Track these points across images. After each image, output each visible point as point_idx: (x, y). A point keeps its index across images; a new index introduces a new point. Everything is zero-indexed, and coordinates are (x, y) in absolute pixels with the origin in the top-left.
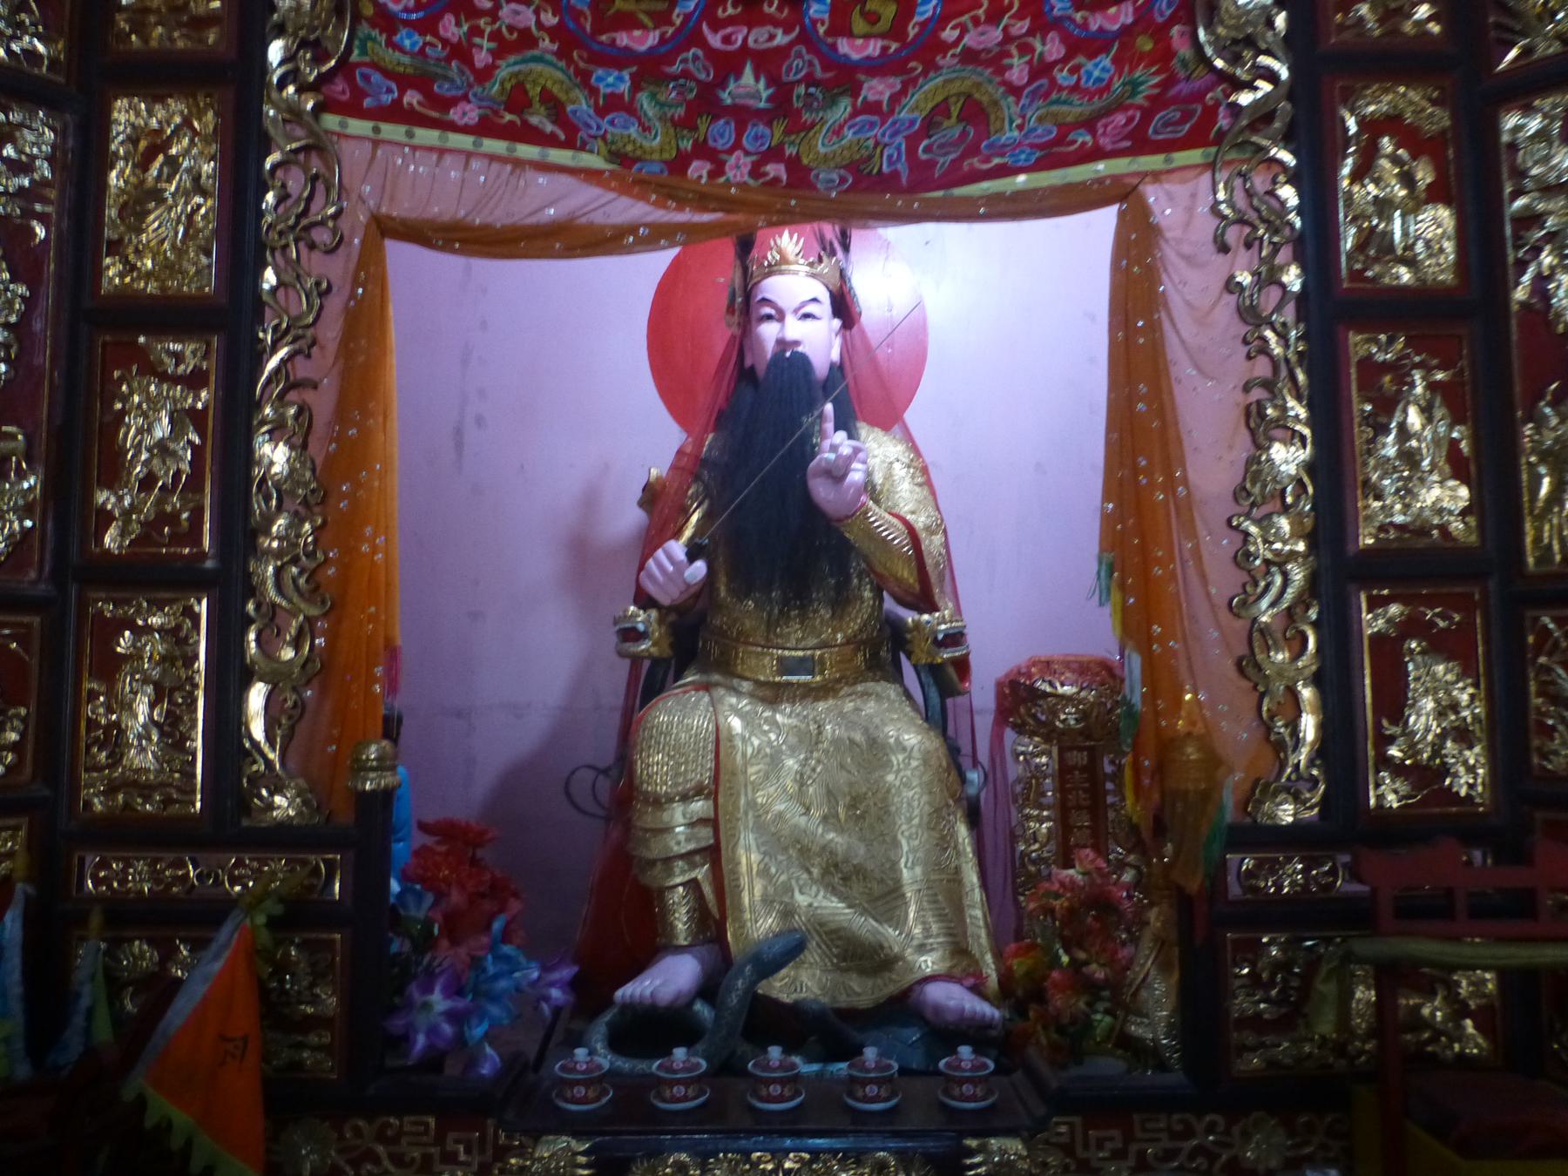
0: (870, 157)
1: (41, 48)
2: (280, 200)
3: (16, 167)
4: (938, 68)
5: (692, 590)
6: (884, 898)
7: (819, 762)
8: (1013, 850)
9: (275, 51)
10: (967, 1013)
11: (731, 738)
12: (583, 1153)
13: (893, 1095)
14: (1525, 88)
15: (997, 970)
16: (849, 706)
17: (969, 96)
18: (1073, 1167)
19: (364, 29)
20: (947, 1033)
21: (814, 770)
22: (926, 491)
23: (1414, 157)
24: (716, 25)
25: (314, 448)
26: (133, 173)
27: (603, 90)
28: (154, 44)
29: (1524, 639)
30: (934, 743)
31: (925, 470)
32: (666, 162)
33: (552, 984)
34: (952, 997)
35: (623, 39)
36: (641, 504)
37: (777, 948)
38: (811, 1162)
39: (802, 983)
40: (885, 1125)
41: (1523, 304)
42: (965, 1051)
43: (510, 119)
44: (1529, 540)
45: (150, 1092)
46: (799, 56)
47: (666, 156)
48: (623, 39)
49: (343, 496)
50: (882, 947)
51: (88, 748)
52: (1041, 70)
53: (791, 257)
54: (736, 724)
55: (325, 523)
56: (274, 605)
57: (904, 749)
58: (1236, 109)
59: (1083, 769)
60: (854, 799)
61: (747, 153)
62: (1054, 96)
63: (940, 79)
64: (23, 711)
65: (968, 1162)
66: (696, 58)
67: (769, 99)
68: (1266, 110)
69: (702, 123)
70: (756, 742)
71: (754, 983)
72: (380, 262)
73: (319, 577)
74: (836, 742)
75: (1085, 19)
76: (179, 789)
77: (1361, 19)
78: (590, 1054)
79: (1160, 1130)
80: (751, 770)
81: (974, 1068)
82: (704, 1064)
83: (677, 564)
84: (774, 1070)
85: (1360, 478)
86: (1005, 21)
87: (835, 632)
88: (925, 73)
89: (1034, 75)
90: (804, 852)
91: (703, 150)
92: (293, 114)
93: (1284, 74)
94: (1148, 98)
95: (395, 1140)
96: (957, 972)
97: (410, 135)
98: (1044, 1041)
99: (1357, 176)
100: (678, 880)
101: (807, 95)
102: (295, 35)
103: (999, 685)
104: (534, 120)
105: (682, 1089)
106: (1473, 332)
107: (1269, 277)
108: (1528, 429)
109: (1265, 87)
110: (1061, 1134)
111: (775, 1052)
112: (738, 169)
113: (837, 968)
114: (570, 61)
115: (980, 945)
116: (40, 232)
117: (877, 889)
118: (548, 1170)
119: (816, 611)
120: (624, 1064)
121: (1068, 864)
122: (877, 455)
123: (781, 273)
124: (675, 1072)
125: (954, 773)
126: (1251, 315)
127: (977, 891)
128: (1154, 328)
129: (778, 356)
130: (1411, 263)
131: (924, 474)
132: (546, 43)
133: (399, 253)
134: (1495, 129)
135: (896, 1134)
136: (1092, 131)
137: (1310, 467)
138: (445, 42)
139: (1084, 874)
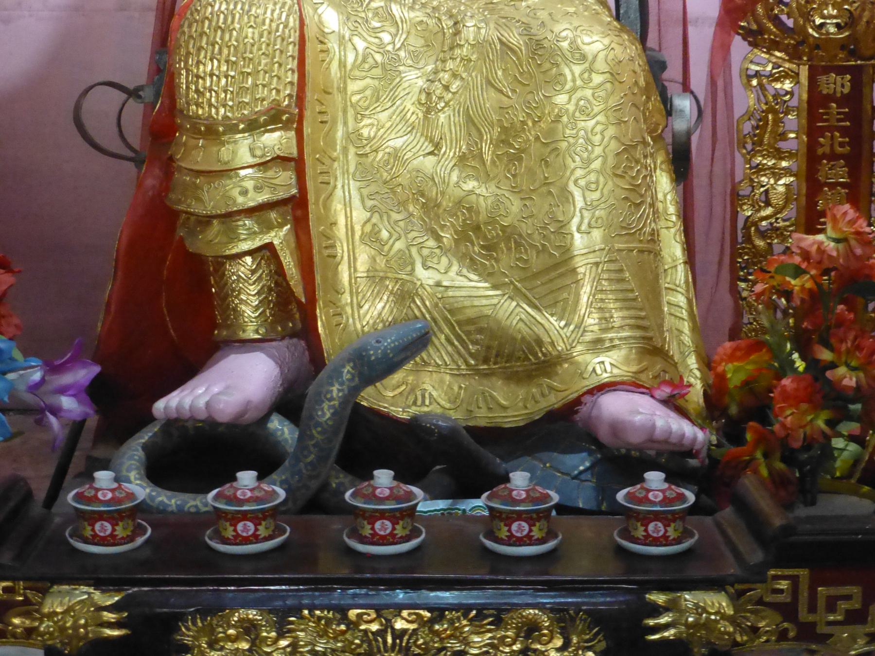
6: (547, 275)
7: (455, 75)
8: (735, 215)
10: (658, 434)
12: (110, 609)
13: (550, 534)
15: (703, 379)
18: (792, 634)
20: (624, 461)
21: (446, 88)
30: (627, 50)
33: (63, 390)
34: (638, 413)
37: (389, 342)
38: (432, 621)
39: (429, 393)
40: (540, 574)
42: (655, 479)
50: (539, 342)
57: (584, 57)
59: (843, 101)
60: (504, 130)
65: (651, 622)
70: (360, 45)
71: (355, 391)
74: (479, 45)
78: (117, 479)
80: (353, 86)
81: (666, 501)
82: (282, 494)
84: (382, 500)
90: (431, 208)
96: (646, 379)
98: (764, 472)
100: (245, 246)
105: (251, 526)
110: (781, 591)
111: (384, 478)
115: (681, 343)
117: (536, 262)
118: (63, 629)
120: (170, 500)
121: (811, 229)
124: (241, 502)
125: (655, 98)
127: (681, 268)
135: (552, 586)
139: (837, 241)
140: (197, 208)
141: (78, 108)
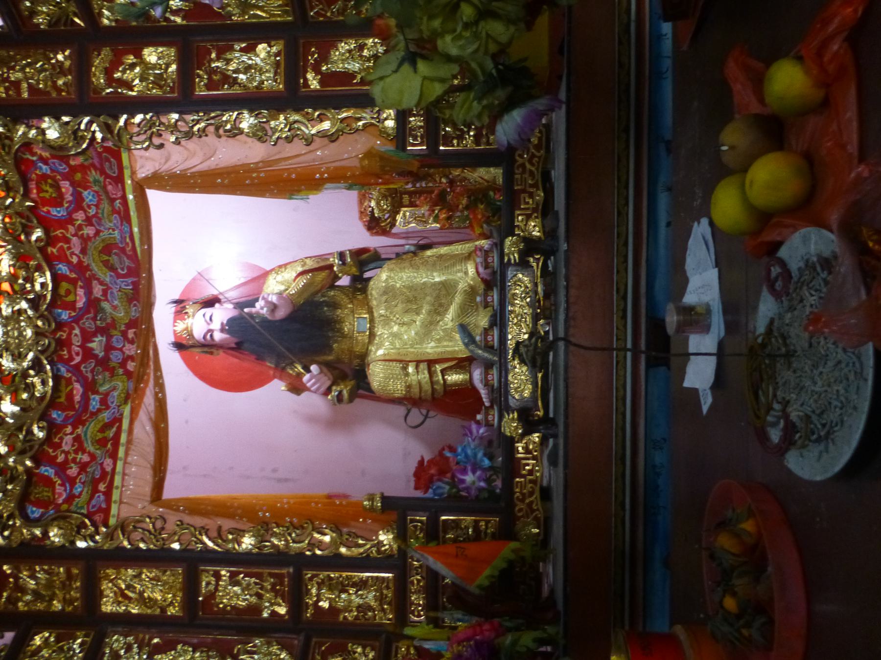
0: (126, 294)
1: (79, 641)
3: (129, 648)
4: (88, 265)
5: (325, 370)
6: (447, 288)
9: (81, 544)
11: (385, 355)
14: (92, 18)
16: (374, 303)
17: (101, 252)
19: (73, 508)
23: (122, 63)
24: (71, 359)
26: (133, 603)
27: (98, 406)
28: (78, 595)
29: (321, 22)
31: (280, 267)
32: (128, 379)
33: (478, 432)
35: (77, 398)
36: (299, 394)
41: (183, 20)
43: (110, 444)
44: (279, 19)
45: (477, 582)
46: (84, 323)
47: (126, 380)
48: (77, 398)
49: (264, 515)
51: (366, 619)
52: (89, 221)
53: (184, 326)
54: (380, 352)
55: (275, 523)
56: (309, 543)
58: (103, 139)
59: (410, 196)
61: (124, 346)
62: (100, 215)
63: (93, 264)
66: (85, 367)
67: (102, 336)
68: (104, 127)
69: (112, 364)
72: (170, 501)
73: (297, 525)
74: (386, 310)
75: (67, 202)
76: (383, 583)
77: (64, 84)
80: (398, 346)
83: (313, 377)
85: (255, 90)
86: (69, 236)
88: (91, 270)
89: (92, 225)
90: (431, 323)
91: (123, 364)
92: (110, 536)
93: (86, 119)
94: (101, 176)
95: (523, 495)
97: (117, 488)
100: (440, 377)
101: (100, 320)
102: (75, 536)
103: (372, 234)
104: (111, 435)
106: (199, 37)
109: (94, 127)
112: (131, 350)
114: (86, 420)
116: (156, 641)
117: (444, 292)
119: (338, 316)
122: (273, 287)
123: (192, 331)
126: (189, 135)
128: (193, 175)
129: (228, 332)
130: (168, 65)
132: (79, 431)
136: (115, 199)
137: (251, 111)
138: (79, 474)
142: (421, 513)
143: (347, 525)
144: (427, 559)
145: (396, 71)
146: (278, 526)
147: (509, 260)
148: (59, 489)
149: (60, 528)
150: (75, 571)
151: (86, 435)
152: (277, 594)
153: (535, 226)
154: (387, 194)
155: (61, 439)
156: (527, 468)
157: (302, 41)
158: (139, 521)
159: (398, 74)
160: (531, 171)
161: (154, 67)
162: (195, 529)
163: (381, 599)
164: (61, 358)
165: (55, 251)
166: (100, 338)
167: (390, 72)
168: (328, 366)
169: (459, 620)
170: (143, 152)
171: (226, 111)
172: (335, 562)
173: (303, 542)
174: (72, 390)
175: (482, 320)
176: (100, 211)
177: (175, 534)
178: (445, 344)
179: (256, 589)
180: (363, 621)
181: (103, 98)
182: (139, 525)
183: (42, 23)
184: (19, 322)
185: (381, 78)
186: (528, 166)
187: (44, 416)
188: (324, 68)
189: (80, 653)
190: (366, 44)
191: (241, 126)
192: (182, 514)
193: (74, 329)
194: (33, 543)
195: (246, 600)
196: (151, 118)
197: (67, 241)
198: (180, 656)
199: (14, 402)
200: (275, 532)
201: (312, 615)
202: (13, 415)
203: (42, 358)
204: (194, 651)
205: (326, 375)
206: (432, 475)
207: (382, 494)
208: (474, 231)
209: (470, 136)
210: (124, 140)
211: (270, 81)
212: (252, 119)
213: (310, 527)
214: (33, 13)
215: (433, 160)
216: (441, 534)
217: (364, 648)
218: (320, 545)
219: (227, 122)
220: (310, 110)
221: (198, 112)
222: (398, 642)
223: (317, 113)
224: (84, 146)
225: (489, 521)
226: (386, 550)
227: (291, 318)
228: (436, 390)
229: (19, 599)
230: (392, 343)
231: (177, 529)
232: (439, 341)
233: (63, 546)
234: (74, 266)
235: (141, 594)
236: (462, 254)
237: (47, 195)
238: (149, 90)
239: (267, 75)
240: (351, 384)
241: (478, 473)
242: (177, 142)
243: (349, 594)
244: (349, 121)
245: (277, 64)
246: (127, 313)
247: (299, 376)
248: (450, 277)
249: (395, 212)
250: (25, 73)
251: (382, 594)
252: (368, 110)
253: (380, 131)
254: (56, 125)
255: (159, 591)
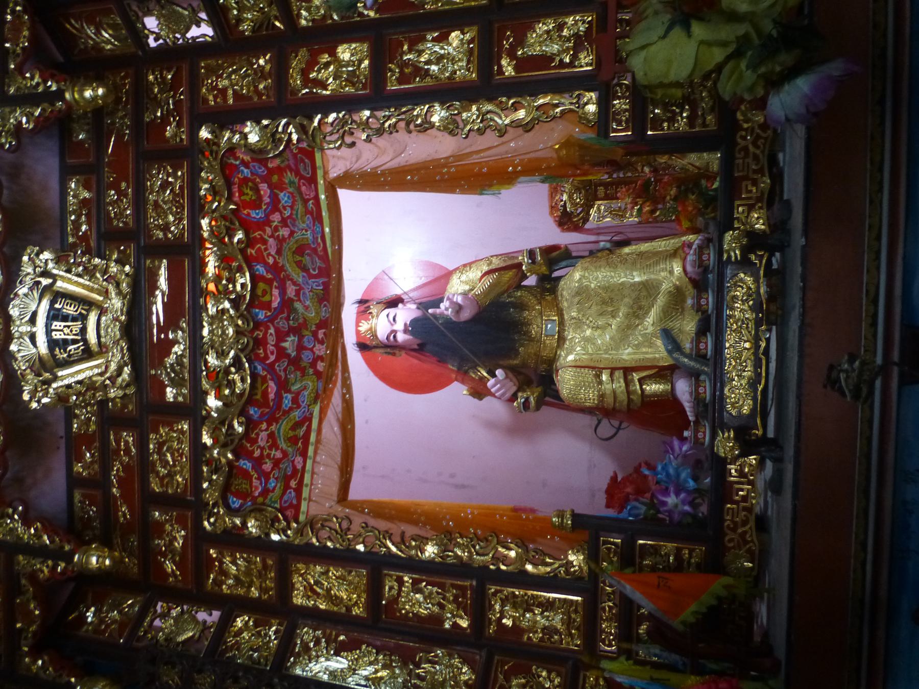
0: (317, 294)
1: (274, 628)
2: (331, 540)
3: (317, 642)
4: (283, 266)
5: (510, 375)
6: (648, 289)
9: (275, 537)
11: (575, 360)
14: (290, 18)
16: (565, 304)
17: (294, 253)
19: (267, 501)
22: (473, 265)
23: (318, 63)
24: (267, 357)
25: (429, 536)
27: (290, 405)
31: (465, 266)
33: (681, 449)
35: (272, 396)
36: (481, 399)
41: (376, 13)
45: (682, 617)
48: (272, 396)
51: (551, 643)
52: (284, 222)
53: (369, 326)
54: (571, 358)
55: (459, 533)
58: (298, 140)
61: (314, 346)
63: (288, 265)
64: (534, 667)
69: (303, 364)
72: (356, 502)
76: (571, 607)
79: (744, 163)
80: (590, 351)
86: (266, 237)
87: (535, 309)
88: (285, 271)
89: (287, 226)
90: (629, 327)
92: (300, 532)
95: (735, 523)
96: (683, 255)
97: (307, 485)
99: (325, 87)
100: (638, 387)
103: (563, 230)
104: (302, 434)
107: (365, 125)
108: (427, 7)
109: (291, 128)
112: (320, 350)
113: (682, 313)
116: (342, 638)
117: (644, 293)
119: (525, 318)
122: (457, 287)
123: (376, 331)
126: (380, 132)
129: (412, 333)
130: (360, 61)
131: (467, 266)
132: (273, 427)
133: (354, 494)
134: (305, 29)
136: (309, 200)
137: (442, 104)
138: (273, 469)
140: (625, 403)
141: (601, 439)
142: (614, 535)
143: (533, 541)
144: (625, 588)
145: (664, 37)
146: (462, 537)
147: (729, 257)
148: (256, 482)
149: (256, 520)
150: (270, 562)
151: (279, 433)
152: (459, 606)
153: (758, 218)
154: (581, 186)
155: (258, 434)
156: (741, 493)
157: (496, 25)
158: (326, 520)
159: (667, 40)
160: (754, 154)
161: (348, 64)
162: (379, 532)
163: (568, 623)
164: (257, 355)
165: (253, 252)
166: (292, 338)
167: (656, 39)
168: (512, 371)
169: (655, 656)
170: (335, 152)
171: (417, 105)
172: (520, 579)
173: (487, 554)
174: (267, 387)
175: (688, 326)
176: (294, 212)
177: (360, 535)
178: (644, 350)
179: (439, 599)
180: (548, 644)
181: (300, 99)
182: (326, 524)
183: (246, 30)
184: (222, 321)
185: (643, 47)
186: (751, 149)
187: (243, 413)
188: (520, 53)
189: (275, 639)
190: (566, 23)
191: (432, 119)
192: (367, 517)
193: (269, 328)
194: (234, 531)
195: (429, 608)
196: (344, 116)
197: (265, 242)
198: (365, 656)
199: (218, 397)
200: (458, 543)
201: (494, 631)
202: (218, 410)
203: (242, 356)
204: (377, 654)
205: (511, 380)
206: (628, 494)
207: (573, 511)
208: (681, 225)
209: (683, 118)
210: (318, 141)
211: (463, 71)
212: (443, 112)
213: (495, 540)
214: (239, 20)
215: (641, 146)
216: (638, 560)
217: (549, 672)
218: (505, 559)
219: (418, 116)
220: (504, 99)
221: (389, 108)
222: (587, 671)
223: (512, 101)
224: (282, 148)
225: (694, 550)
226: (575, 571)
227: (475, 320)
228: (632, 400)
229: (223, 583)
230: (583, 348)
231: (362, 531)
232: (637, 346)
233: (259, 537)
234: (271, 267)
235: (329, 590)
236: (667, 251)
237: (247, 198)
238: (342, 88)
239: (460, 64)
240: (538, 391)
241: (682, 495)
242: (368, 140)
243: (534, 614)
244: (546, 108)
245: (470, 52)
246: (317, 313)
247: (483, 380)
248: (652, 276)
249: (588, 206)
250: (231, 80)
251: (570, 617)
252: (567, 95)
253: (580, 117)
254: (257, 129)
255: (343, 589)
